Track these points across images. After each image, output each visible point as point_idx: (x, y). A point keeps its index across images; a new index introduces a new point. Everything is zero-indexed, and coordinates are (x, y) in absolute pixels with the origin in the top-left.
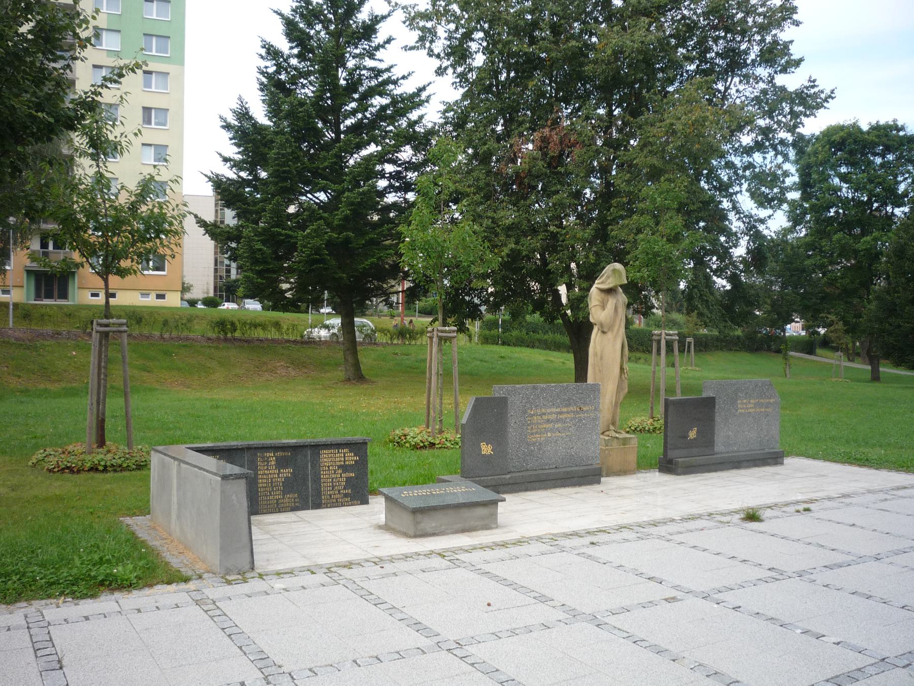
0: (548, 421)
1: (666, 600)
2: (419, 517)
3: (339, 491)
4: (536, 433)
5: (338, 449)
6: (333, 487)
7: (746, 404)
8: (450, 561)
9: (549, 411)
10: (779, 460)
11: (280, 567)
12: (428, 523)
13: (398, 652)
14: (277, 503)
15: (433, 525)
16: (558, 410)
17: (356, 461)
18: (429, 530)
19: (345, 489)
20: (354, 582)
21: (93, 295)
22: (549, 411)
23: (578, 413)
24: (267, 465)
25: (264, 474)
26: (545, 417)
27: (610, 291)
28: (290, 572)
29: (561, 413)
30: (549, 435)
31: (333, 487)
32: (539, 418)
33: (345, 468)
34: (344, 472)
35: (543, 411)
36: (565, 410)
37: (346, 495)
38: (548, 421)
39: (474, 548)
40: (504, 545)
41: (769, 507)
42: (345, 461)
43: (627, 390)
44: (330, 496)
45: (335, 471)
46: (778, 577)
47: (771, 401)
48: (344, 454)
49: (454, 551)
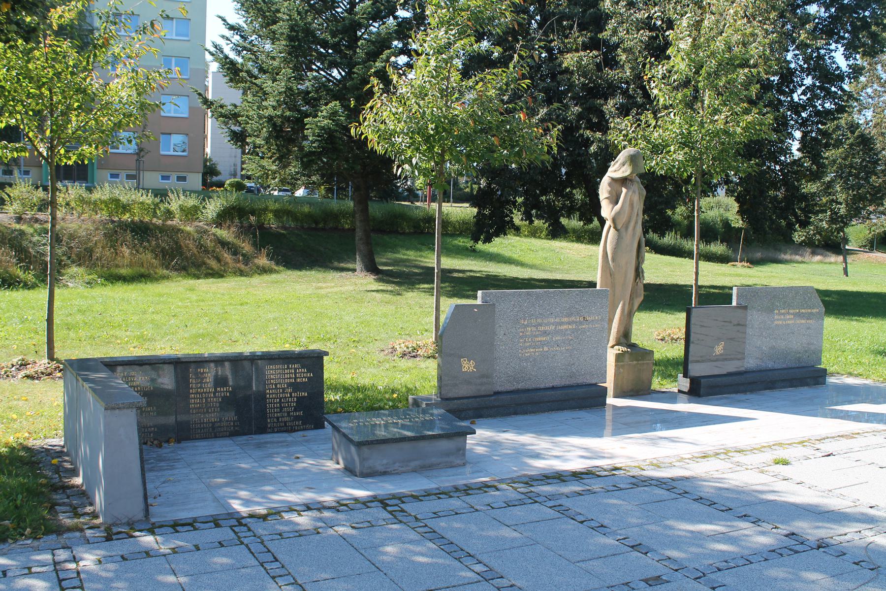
0: (545, 333)
1: (646, 581)
2: (365, 450)
3: (288, 413)
4: (530, 347)
5: (288, 364)
6: (281, 408)
7: (783, 314)
8: (391, 512)
9: (545, 321)
10: (821, 380)
11: (184, 515)
12: (378, 459)
13: (489, 505)
14: (213, 428)
15: (385, 462)
16: (557, 320)
17: (309, 378)
18: (380, 468)
19: (295, 410)
20: (262, 542)
21: (164, 178)
22: (545, 321)
23: (581, 323)
24: (201, 383)
25: (197, 393)
26: (540, 328)
27: (624, 181)
28: (192, 524)
29: (562, 324)
30: (546, 349)
31: (281, 408)
32: (534, 329)
33: (295, 386)
34: (295, 391)
35: (539, 321)
36: (566, 320)
37: (297, 418)
38: (545, 333)
39: (428, 494)
40: (467, 490)
41: (799, 443)
42: (296, 378)
43: (642, 298)
44: (278, 418)
45: (284, 389)
46: (797, 548)
47: (814, 311)
48: (295, 369)
49: (401, 498)
